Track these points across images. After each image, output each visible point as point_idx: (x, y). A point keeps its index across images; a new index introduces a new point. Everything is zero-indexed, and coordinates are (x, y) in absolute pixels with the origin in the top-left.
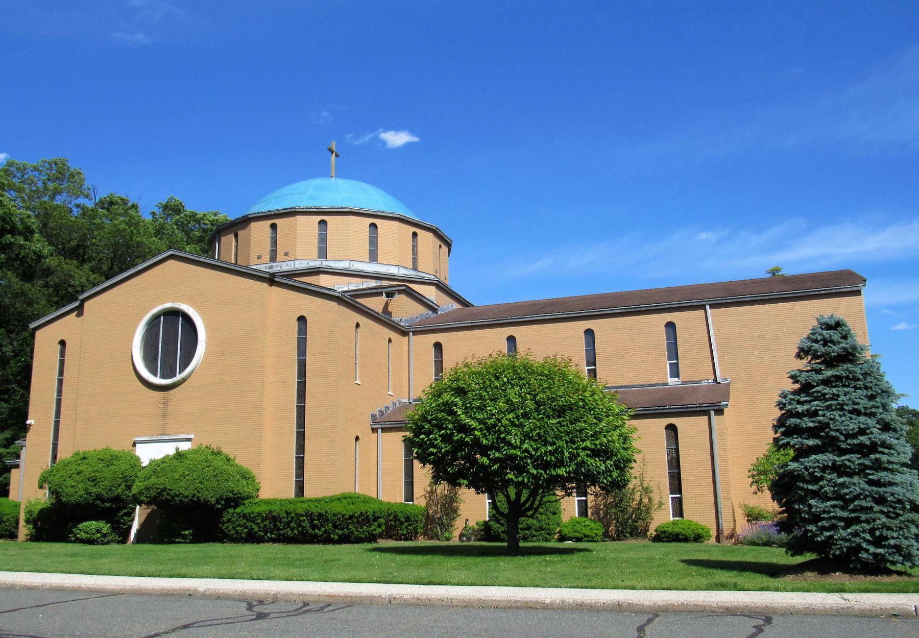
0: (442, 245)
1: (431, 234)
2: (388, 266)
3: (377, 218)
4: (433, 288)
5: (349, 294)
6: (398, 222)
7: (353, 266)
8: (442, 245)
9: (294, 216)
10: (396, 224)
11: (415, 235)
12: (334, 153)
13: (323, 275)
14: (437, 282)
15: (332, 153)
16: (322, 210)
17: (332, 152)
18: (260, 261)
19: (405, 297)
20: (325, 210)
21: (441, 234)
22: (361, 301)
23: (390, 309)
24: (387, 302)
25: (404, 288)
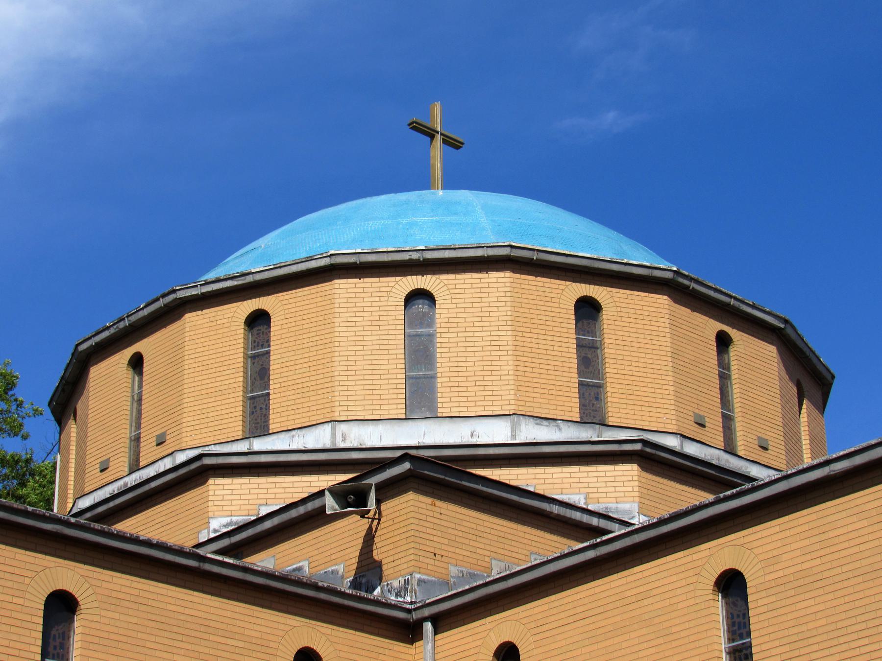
0: (733, 333)
1: (661, 302)
2: (473, 421)
3: (433, 273)
4: (631, 471)
5: (88, 515)
6: (508, 274)
7: (344, 440)
8: (733, 333)
9: (179, 317)
10: (503, 278)
11: (723, 342)
12: (438, 139)
13: (220, 481)
14: (638, 447)
15: (432, 137)
16: (250, 279)
17: (431, 134)
18: (108, 476)
19: (428, 500)
20: (258, 277)
21: (711, 293)
22: (128, 526)
23: (377, 555)
24: (370, 528)
25: (407, 466)
